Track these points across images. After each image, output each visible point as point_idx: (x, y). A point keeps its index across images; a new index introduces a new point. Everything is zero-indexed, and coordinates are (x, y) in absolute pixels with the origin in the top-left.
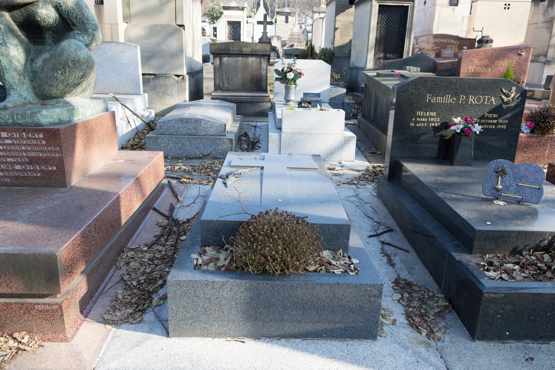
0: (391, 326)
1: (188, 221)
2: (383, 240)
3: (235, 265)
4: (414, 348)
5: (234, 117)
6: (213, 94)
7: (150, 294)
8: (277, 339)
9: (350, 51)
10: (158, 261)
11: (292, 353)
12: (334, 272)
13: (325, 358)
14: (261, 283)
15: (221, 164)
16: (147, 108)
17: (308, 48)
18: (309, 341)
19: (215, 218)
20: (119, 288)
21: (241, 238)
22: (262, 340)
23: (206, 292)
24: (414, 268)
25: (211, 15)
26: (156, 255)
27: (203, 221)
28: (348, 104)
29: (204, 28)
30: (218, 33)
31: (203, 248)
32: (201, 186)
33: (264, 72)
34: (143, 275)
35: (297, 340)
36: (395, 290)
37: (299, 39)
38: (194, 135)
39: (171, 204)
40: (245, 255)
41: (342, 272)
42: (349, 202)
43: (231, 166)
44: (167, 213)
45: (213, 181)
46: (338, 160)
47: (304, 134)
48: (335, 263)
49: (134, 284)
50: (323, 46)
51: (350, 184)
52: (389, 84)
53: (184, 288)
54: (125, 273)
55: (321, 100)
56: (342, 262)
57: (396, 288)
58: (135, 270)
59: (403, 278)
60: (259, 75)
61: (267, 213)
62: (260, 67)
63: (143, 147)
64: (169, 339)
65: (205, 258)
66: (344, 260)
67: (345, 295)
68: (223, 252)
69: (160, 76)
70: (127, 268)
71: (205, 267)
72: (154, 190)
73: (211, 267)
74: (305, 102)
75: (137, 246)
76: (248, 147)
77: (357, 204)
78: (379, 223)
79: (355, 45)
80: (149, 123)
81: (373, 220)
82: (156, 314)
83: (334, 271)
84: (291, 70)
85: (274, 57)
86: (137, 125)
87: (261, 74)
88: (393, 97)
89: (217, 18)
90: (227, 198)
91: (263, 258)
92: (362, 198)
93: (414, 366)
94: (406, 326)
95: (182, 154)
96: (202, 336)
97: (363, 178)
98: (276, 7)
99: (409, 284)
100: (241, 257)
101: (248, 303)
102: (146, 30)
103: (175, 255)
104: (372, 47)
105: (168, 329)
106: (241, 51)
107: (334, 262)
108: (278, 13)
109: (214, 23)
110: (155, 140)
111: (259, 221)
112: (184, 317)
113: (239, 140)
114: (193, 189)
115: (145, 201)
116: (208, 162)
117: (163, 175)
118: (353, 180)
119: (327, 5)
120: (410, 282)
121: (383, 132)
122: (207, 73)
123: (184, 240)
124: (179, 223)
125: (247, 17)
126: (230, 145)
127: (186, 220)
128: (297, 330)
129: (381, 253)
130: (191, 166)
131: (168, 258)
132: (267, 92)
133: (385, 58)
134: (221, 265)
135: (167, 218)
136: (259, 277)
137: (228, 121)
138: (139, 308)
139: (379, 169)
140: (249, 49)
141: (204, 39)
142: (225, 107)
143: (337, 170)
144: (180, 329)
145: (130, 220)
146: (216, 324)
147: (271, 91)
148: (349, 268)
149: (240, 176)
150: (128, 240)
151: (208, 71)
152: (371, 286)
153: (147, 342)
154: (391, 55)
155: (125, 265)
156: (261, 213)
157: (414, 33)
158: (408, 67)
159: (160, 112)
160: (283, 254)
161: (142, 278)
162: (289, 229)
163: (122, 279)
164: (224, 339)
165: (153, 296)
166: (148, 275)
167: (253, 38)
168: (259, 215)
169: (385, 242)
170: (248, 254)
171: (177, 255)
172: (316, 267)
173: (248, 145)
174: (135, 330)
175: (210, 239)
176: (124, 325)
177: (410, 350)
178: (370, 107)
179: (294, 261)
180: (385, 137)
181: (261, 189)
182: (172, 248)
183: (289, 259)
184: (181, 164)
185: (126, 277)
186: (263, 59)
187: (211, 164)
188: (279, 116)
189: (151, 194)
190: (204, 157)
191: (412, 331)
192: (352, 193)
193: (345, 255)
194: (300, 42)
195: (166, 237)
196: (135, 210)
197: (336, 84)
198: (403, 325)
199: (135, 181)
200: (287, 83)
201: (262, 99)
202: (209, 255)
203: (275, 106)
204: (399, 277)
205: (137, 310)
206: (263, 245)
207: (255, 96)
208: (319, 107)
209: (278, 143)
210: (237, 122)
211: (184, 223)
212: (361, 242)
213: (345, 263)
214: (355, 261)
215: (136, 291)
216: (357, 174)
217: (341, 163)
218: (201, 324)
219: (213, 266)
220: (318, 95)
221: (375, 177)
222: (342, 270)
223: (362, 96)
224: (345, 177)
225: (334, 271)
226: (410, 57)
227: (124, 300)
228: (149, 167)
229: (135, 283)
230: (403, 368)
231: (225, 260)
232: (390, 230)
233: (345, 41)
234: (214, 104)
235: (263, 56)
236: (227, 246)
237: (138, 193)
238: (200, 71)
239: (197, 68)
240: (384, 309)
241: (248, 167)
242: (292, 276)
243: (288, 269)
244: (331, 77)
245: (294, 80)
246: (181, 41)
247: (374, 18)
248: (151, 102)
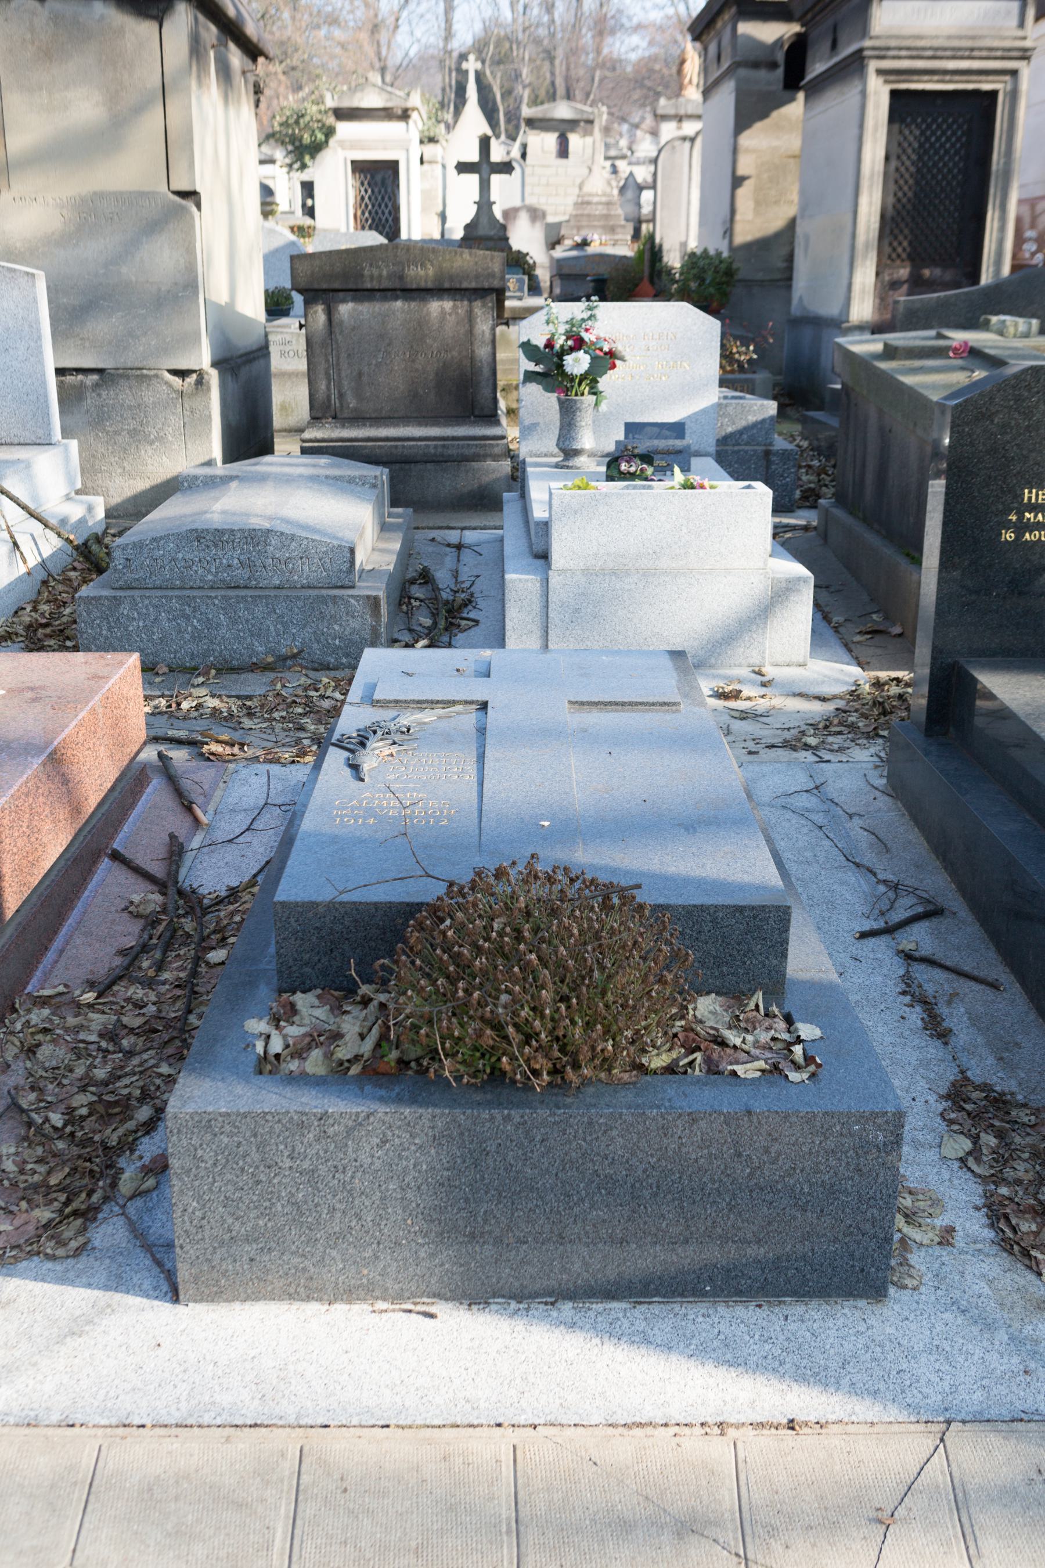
0: (937, 1250)
1: (233, 894)
2: (908, 946)
3: (394, 1055)
4: (1017, 1325)
5: (381, 516)
6: (307, 435)
7: (111, 1153)
8: (546, 1303)
9: (790, 258)
10: (132, 1039)
11: (596, 1350)
12: (734, 1073)
13: (710, 1367)
14: (485, 1115)
15: (344, 685)
16: (77, 492)
17: (640, 253)
18: (656, 1309)
19: (325, 894)
20: (6, 1136)
21: (413, 963)
22: (493, 1307)
23: (301, 1149)
24: (1017, 1045)
25: (294, 139)
26: (125, 1020)
27: (283, 904)
28: (785, 454)
29: (270, 183)
30: (320, 202)
31: (285, 995)
32: (275, 769)
33: (482, 352)
34: (83, 1089)
35: (615, 1305)
36: (951, 1122)
37: (607, 217)
38: (246, 587)
39: (172, 837)
40: (430, 1022)
41: (763, 1071)
42: (789, 815)
43: (376, 704)
44: (157, 869)
45: (314, 748)
46: (752, 661)
47: (627, 573)
48: (738, 1041)
49: (53, 1122)
50: (693, 245)
51: (794, 749)
52: (926, 386)
53: (226, 1140)
54: (22, 1082)
55: (689, 446)
56: (764, 1037)
57: (953, 1116)
58: (56, 1074)
59: (978, 1080)
60: (467, 363)
61: (500, 874)
62: (471, 332)
63: (67, 632)
64: (180, 1308)
65: (294, 1031)
66: (769, 1029)
67: (773, 1150)
68: (355, 1010)
69: (121, 376)
70: (29, 1064)
71: (294, 1065)
72: (112, 789)
73: (315, 1062)
74: (631, 457)
75: (61, 989)
76: (435, 624)
77: (819, 818)
78: (895, 887)
79: (807, 239)
80: (85, 544)
81: (875, 874)
82: (131, 1223)
83: (735, 1067)
84: (579, 344)
85: (521, 289)
86: (45, 556)
87: (472, 359)
88: (941, 429)
89: (316, 149)
90: (365, 818)
91: (488, 1032)
92: (834, 796)
93: (1014, 1388)
94: (986, 1247)
95: (206, 654)
96: (292, 1297)
97: (840, 724)
98: (525, 100)
99: (1000, 1102)
100: (415, 1028)
101: (442, 1185)
102: (65, 212)
103: (193, 1019)
104: (867, 246)
105: (175, 1274)
106: (401, 278)
107: (734, 1038)
108: (531, 123)
109: (304, 166)
110: (110, 609)
111: (475, 905)
112: (227, 1237)
113: (402, 597)
114: (245, 782)
115: (80, 830)
116: (294, 682)
117: (142, 735)
118: (803, 733)
119: (707, 93)
120: (1002, 1094)
121: (908, 555)
122: (283, 354)
123: (223, 963)
124: (200, 902)
125: (422, 142)
127: (224, 894)
128: (612, 1273)
129: (904, 993)
130: (238, 697)
131: (167, 1027)
132: (497, 423)
133: (917, 284)
134: (348, 1057)
135: (161, 885)
136: (478, 1097)
137: (361, 535)
138: (75, 1205)
139: (894, 690)
140: (431, 271)
141: (271, 232)
142: (351, 481)
143: (749, 699)
144: (215, 1275)
145: (34, 899)
146: (338, 1257)
147: (511, 412)
148: (786, 1058)
149: (405, 737)
150: (29, 967)
151: (287, 348)
152: (862, 1118)
153: (104, 1322)
154: (938, 271)
155: (23, 1056)
156: (479, 874)
157: (1022, 187)
158: (994, 319)
159: (124, 502)
160: (557, 1016)
161: (81, 1101)
162: (575, 931)
163: (15, 1106)
164: (366, 1307)
165: (122, 1162)
166: (102, 1089)
167: (443, 217)
168: (473, 881)
169: (917, 954)
170: (440, 1020)
171: (200, 1017)
172: (674, 1055)
173: (434, 615)
174: (62, 1280)
175: (307, 964)
176: (25, 1263)
177: (1002, 1331)
178: (864, 466)
179: (596, 1041)
180: (915, 577)
181: (481, 784)
182: (179, 992)
183: (578, 1031)
184: (203, 691)
185: (27, 1100)
186: (478, 304)
187: (306, 689)
188: (539, 513)
189: (100, 805)
190: (280, 663)
191: (1007, 1265)
192: (802, 780)
193: (775, 1009)
194: (612, 230)
195: (158, 955)
196: (47, 864)
197: (740, 381)
198: (979, 1246)
199: (44, 764)
200: (567, 391)
201: (482, 446)
202: (307, 1021)
203: (524, 471)
204: (967, 1079)
205: (68, 1210)
206: (488, 986)
207: (454, 438)
208: (679, 476)
209: (537, 606)
210: (393, 535)
211: (217, 904)
212: (827, 963)
213: (774, 1039)
214: (807, 1031)
215: (61, 1145)
216: (817, 707)
217: (760, 673)
218: (285, 1258)
219: (321, 1058)
220: (678, 429)
221: (882, 719)
222: (761, 1064)
223: (834, 422)
224: (775, 722)
225: (735, 1067)
226: (1008, 281)
227: (23, 1177)
228: (93, 712)
229: (57, 1119)
230: (979, 1393)
231: (362, 1037)
232: (932, 912)
233: (774, 222)
234: (310, 471)
235: (479, 293)
236: (365, 989)
237: (57, 805)
238: (260, 349)
239: (248, 341)
240: (910, 1193)
241: (433, 703)
242: (591, 1090)
243: (576, 1066)
244: (723, 356)
245: (591, 378)
246: (190, 250)
247: (875, 141)
248: (89, 467)
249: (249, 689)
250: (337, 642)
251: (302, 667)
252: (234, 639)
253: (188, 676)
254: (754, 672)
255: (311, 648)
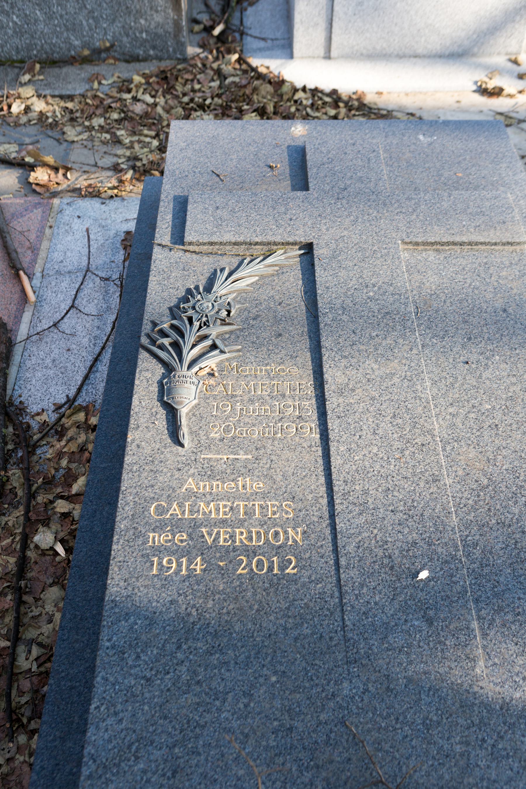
46: (510, 50)
95: (29, 47)
126: (171, 13)
143: (510, 96)
217: (515, 62)
249: (70, 87)
250: (144, 35)
251: (116, 59)
252: (52, 33)
253: (16, 71)
254: (510, 60)
255: (121, 41)
